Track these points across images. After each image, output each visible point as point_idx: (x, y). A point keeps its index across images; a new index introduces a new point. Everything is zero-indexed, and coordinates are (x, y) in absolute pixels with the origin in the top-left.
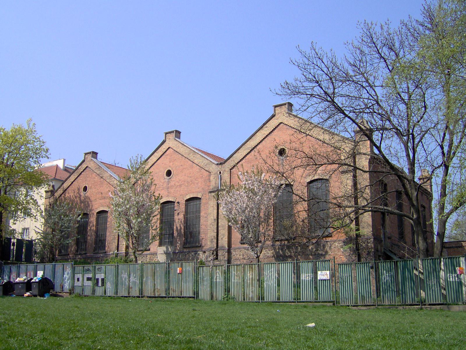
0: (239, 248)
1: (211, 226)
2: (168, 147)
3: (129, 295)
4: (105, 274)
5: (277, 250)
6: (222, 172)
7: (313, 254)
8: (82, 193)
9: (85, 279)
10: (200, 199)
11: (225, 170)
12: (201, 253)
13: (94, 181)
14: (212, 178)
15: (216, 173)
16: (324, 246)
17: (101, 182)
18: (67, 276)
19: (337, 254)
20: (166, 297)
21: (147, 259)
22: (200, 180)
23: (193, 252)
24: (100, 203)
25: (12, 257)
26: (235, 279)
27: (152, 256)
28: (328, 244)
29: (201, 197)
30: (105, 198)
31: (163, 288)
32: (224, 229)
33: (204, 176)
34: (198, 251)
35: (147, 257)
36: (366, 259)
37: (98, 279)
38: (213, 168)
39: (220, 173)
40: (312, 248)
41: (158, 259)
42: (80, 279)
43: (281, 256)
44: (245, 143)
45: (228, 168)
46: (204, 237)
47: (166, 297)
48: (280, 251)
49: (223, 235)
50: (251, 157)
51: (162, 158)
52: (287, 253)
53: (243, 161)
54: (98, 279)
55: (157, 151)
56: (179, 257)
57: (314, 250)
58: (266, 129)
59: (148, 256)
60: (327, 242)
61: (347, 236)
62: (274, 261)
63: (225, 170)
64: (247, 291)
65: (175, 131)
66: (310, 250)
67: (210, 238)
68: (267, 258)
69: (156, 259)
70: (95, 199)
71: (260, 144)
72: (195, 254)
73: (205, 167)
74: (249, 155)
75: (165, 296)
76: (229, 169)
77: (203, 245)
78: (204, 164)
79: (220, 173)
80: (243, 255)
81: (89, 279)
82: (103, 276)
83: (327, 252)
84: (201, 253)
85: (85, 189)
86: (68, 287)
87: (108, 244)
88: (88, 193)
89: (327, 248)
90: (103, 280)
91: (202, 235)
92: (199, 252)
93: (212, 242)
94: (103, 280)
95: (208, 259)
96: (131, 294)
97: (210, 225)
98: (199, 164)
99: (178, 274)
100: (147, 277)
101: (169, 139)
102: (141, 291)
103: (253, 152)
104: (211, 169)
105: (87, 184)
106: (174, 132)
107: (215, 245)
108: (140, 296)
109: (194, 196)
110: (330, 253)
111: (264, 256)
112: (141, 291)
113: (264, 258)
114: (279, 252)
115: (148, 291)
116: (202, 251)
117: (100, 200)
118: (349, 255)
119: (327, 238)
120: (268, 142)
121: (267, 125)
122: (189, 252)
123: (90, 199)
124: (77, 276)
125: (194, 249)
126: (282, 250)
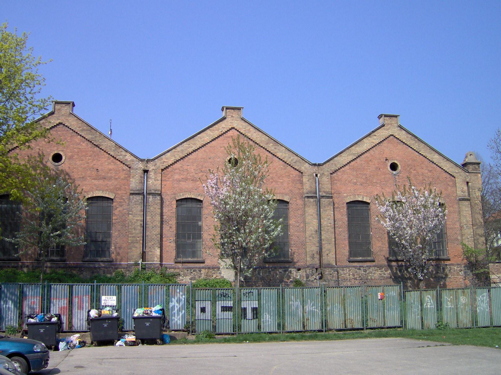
0: (346, 267)
1: (311, 238)
2: (230, 127)
3: (304, 329)
4: (259, 300)
5: (395, 271)
6: (319, 175)
7: (433, 276)
8: (50, 164)
9: (219, 309)
10: (288, 203)
11: (323, 174)
12: (294, 271)
13: (80, 149)
14: (305, 179)
15: (312, 174)
16: (444, 269)
17: (94, 152)
18: (176, 304)
19: (457, 277)
20: (362, 329)
21: (201, 274)
22: (286, 179)
23: (281, 268)
24: (95, 185)
25: (173, 270)
26: (448, 305)
27: (210, 270)
28: (447, 267)
29: (288, 201)
30: (105, 178)
31: (360, 318)
32: (329, 244)
33: (291, 176)
34: (289, 268)
35: (200, 271)
36: (484, 283)
37: (245, 309)
38: (306, 168)
39: (316, 175)
40: (432, 270)
41: (222, 275)
42: (207, 310)
43: (399, 277)
44: (350, 148)
45: (328, 171)
46: (296, 251)
47: (362, 329)
48: (398, 272)
49: (329, 250)
50: (356, 165)
51: (219, 139)
52: (406, 274)
53: (347, 167)
54: (245, 309)
55: (210, 129)
56: (259, 273)
57: (434, 272)
58: (375, 137)
59: (203, 271)
60: (446, 265)
61: (468, 261)
62: (392, 283)
63: (323, 174)
64: (460, 317)
65: (71, 103)
66: (430, 272)
67: (311, 253)
68: (383, 279)
69: (218, 275)
70: (83, 178)
71: (368, 152)
72: (285, 271)
73: (293, 164)
74: (354, 162)
75: (361, 327)
76: (329, 173)
77: (295, 260)
78: (292, 160)
79: (316, 175)
80: (353, 275)
81: (225, 309)
82: (255, 304)
83: (446, 275)
84: (294, 271)
85: (57, 158)
86: (180, 322)
87: (115, 248)
88: (64, 165)
89: (447, 271)
90: (255, 310)
91: (293, 248)
92: (290, 269)
93: (313, 257)
94: (255, 310)
95: (310, 278)
96: (307, 328)
97: (309, 237)
98: (284, 158)
99: (380, 300)
100: (333, 304)
101: (232, 117)
102: (324, 323)
103: (358, 160)
104: (303, 169)
105: (62, 151)
106: (70, 103)
107: (318, 262)
108: (324, 329)
109: (94, 196)
110: (450, 276)
111: (380, 277)
112: (324, 323)
113: (381, 279)
114: (396, 273)
115: (336, 322)
116: (295, 268)
117: (94, 179)
118: (472, 279)
119: (445, 262)
120: (377, 152)
121: (375, 133)
122: (275, 268)
123: (69, 176)
124: (199, 305)
125: (282, 265)
126: (400, 271)
